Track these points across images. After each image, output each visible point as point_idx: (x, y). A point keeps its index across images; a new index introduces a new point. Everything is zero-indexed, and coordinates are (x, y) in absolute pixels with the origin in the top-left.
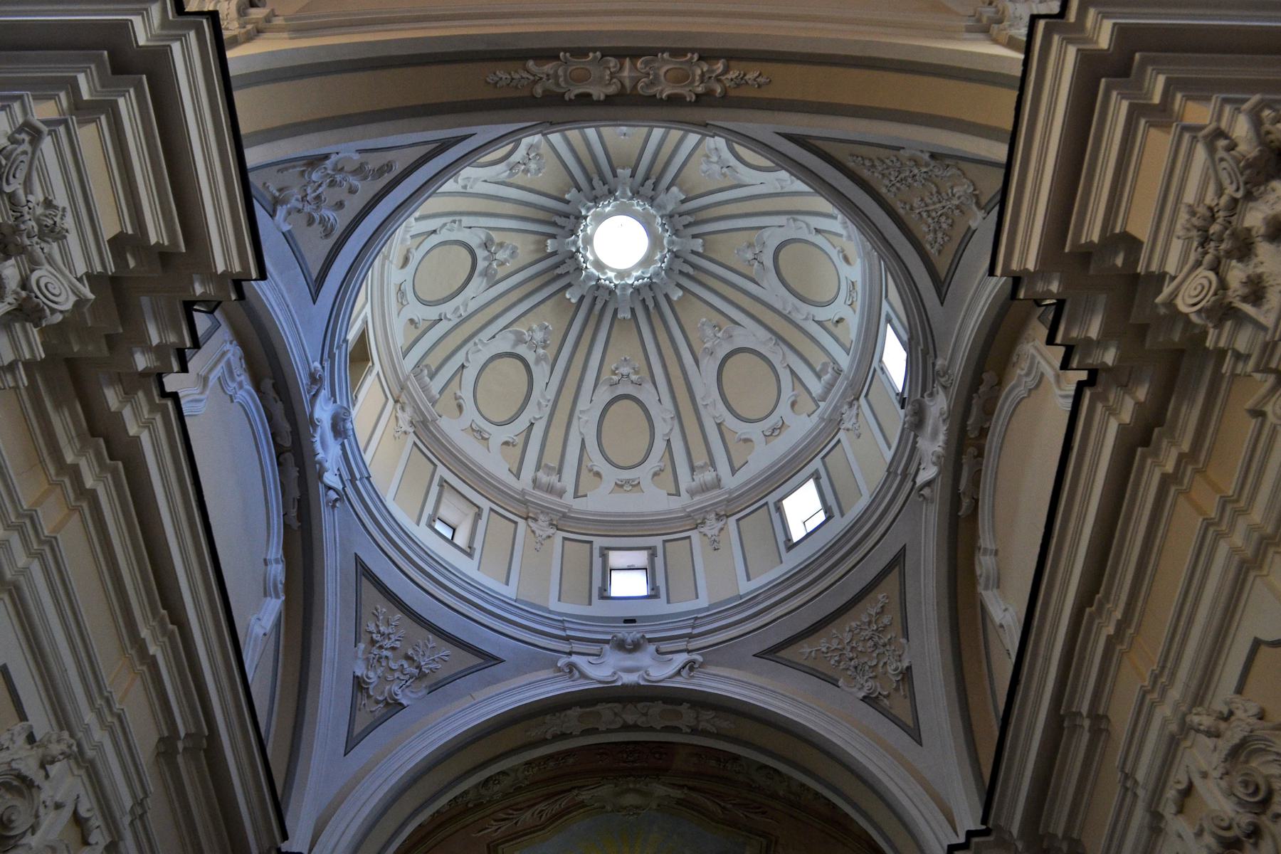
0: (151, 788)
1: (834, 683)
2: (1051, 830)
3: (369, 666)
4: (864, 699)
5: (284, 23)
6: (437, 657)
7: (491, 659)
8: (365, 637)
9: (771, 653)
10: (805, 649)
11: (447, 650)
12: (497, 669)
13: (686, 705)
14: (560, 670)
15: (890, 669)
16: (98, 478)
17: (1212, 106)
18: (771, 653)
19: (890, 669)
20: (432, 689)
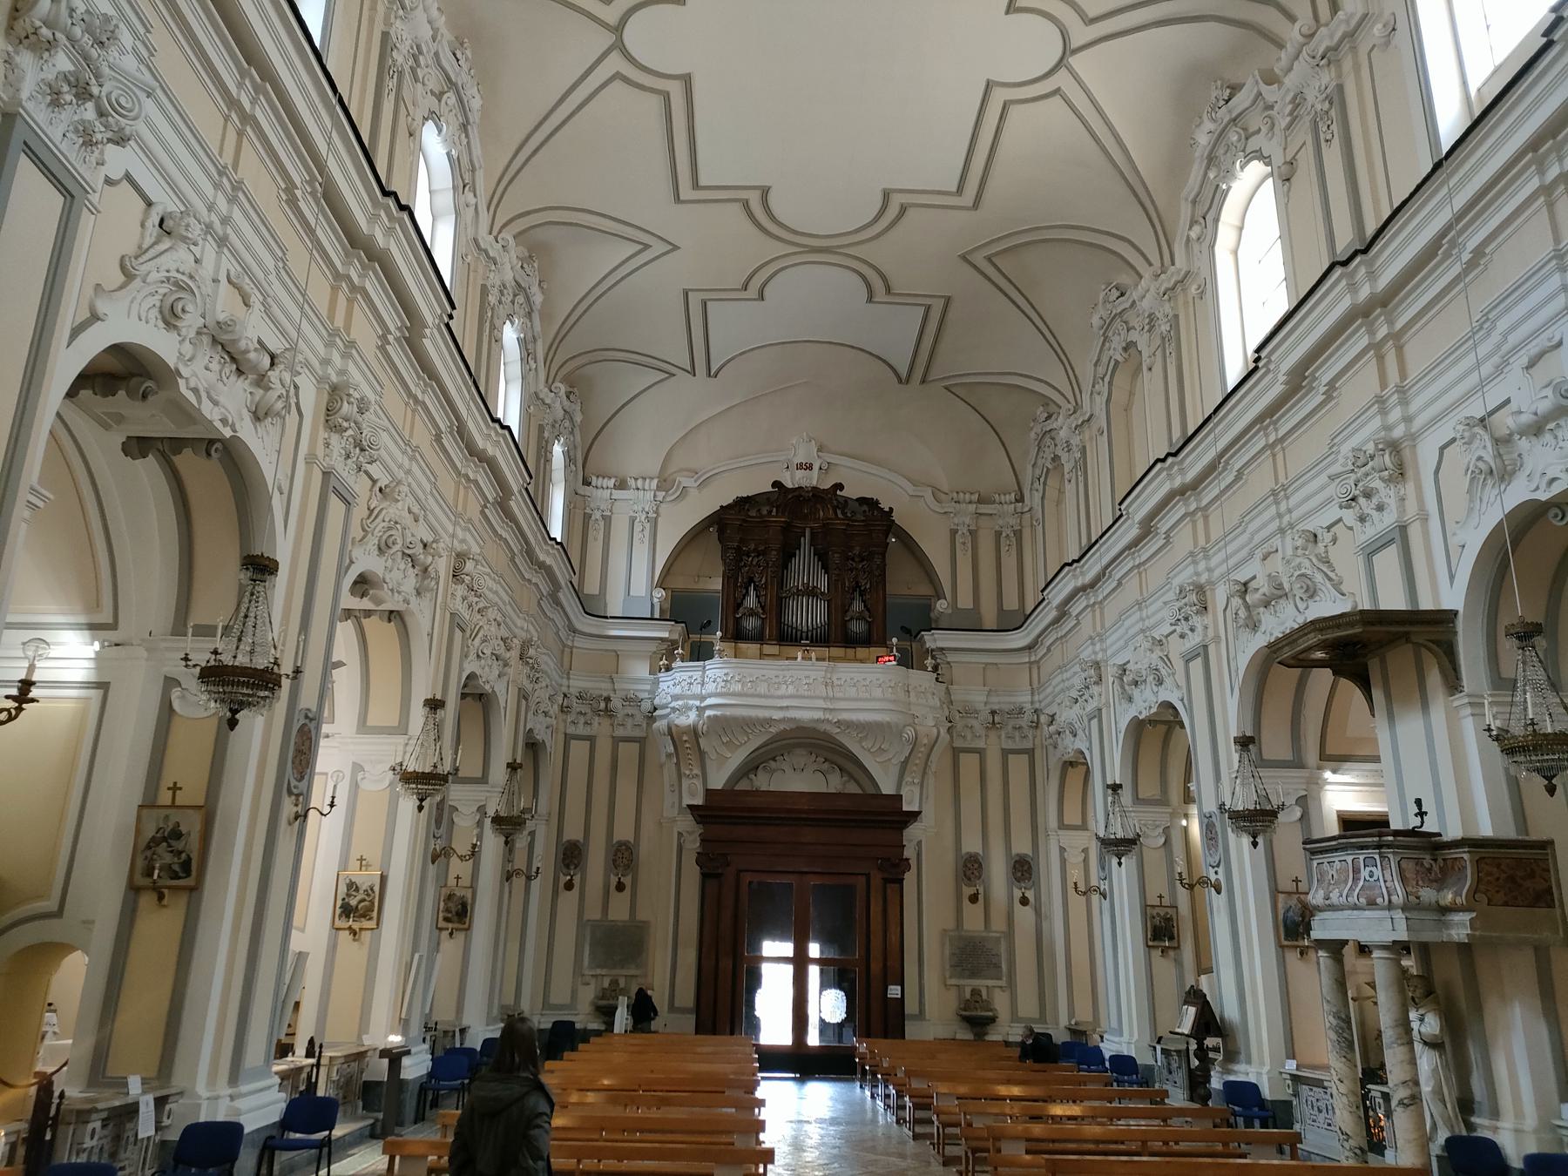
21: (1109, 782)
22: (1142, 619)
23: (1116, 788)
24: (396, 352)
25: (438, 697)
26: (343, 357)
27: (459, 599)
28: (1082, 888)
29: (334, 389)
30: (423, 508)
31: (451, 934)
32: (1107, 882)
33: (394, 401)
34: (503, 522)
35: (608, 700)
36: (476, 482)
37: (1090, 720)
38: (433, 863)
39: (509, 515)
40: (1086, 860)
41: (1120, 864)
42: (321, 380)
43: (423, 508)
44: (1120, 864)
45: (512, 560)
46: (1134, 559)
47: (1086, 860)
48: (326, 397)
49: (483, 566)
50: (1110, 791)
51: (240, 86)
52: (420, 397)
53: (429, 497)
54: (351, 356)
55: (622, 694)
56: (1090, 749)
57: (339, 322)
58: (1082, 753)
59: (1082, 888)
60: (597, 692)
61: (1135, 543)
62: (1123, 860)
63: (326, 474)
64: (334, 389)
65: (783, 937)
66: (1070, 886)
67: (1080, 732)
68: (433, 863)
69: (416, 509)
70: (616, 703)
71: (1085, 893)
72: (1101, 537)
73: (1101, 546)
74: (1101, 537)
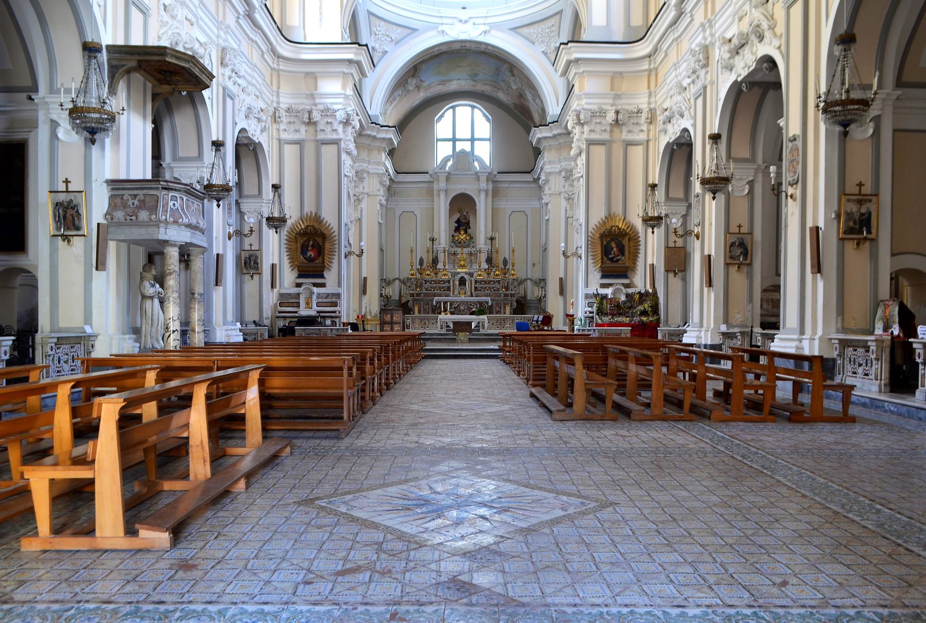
0: (264, 50)
1: (534, 44)
2: (688, 229)
3: (375, 41)
4: (543, 52)
5: (215, 253)
6: (396, 33)
7: (414, 30)
8: (373, 33)
9: (514, 29)
10: (525, 31)
11: (399, 30)
12: (417, 33)
13: (506, 66)
14: (439, 32)
15: (552, 45)
16: (255, 36)
17: (663, 225)
18: (514, 29)
19: (552, 45)
20: (397, 43)
21: (650, 182)
22: (676, 76)
23: (654, 186)
24: (244, 23)
25: (221, 139)
26: (224, 33)
27: (227, 78)
28: (680, 232)
29: (224, 49)
30: (195, 16)
31: (252, 277)
32: (700, 228)
33: (245, 47)
34: (253, 29)
35: (310, 112)
36: (256, 42)
37: (696, 99)
38: (229, 239)
39: (256, 25)
40: (751, 192)
41: (653, 232)
42: (217, 45)
43: (195, 16)
44: (653, 232)
45: (263, 56)
46: (674, 34)
47: (751, 192)
48: (220, 53)
49: (241, 57)
50: (650, 188)
51: (273, 63)
52: (254, 38)
53: (199, 9)
54: (228, 33)
55: (321, 107)
56: (694, 125)
57: (221, 18)
58: (688, 131)
59: (680, 232)
60: (302, 107)
61: (674, 22)
62: (655, 230)
63: (224, 89)
64: (224, 49)
65: (494, 154)
66: (671, 230)
67: (686, 113)
68: (229, 239)
69: (190, 17)
70: (316, 116)
71: (682, 236)
72: (654, 21)
73: (654, 29)
74: (654, 21)
